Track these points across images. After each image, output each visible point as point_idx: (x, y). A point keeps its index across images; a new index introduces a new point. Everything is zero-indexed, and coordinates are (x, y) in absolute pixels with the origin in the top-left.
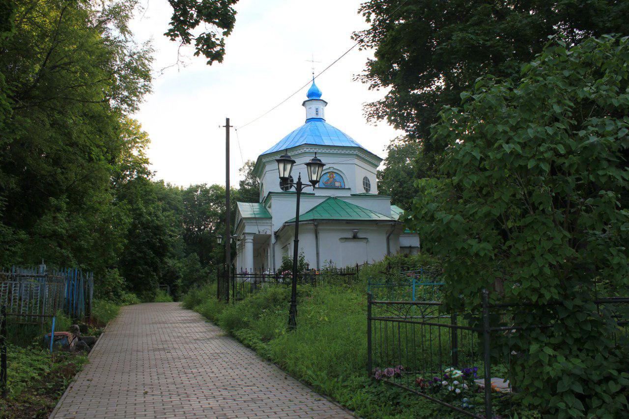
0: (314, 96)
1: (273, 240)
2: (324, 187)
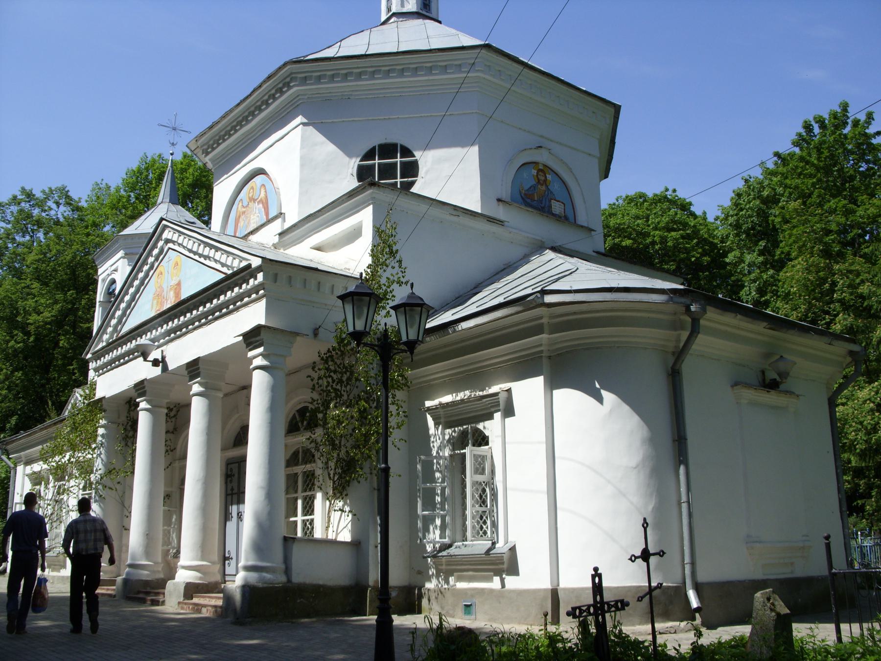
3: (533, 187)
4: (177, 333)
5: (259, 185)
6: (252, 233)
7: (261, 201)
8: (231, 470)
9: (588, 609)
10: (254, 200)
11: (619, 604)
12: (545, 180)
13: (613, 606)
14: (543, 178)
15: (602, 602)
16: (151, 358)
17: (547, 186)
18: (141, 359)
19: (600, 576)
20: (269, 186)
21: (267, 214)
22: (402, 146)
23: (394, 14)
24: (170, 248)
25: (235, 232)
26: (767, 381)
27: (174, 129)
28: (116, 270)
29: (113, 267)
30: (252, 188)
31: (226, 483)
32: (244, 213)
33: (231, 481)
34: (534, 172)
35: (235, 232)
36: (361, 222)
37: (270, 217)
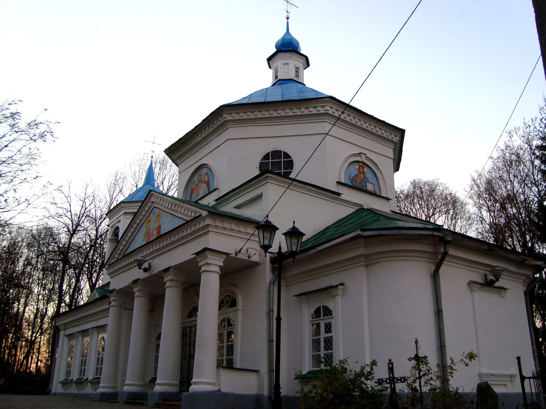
0: (287, 47)
1: (267, 274)
2: (350, 184)
3: (357, 175)
4: (161, 252)
5: (204, 174)
6: (200, 199)
7: (205, 182)
8: (186, 332)
9: (386, 380)
10: (202, 182)
11: (402, 380)
12: (364, 171)
13: (399, 380)
14: (362, 170)
15: (394, 378)
16: (143, 267)
17: (364, 175)
18: (137, 267)
19: (392, 364)
20: (210, 174)
21: (209, 189)
22: (284, 152)
23: (279, 80)
24: (154, 207)
25: (191, 199)
26: (488, 281)
27: (154, 143)
28: (119, 221)
29: (118, 220)
30: (201, 175)
31: (183, 339)
32: (196, 188)
33: (186, 338)
34: (357, 167)
35: (191, 199)
36: (262, 193)
37: (211, 191)
